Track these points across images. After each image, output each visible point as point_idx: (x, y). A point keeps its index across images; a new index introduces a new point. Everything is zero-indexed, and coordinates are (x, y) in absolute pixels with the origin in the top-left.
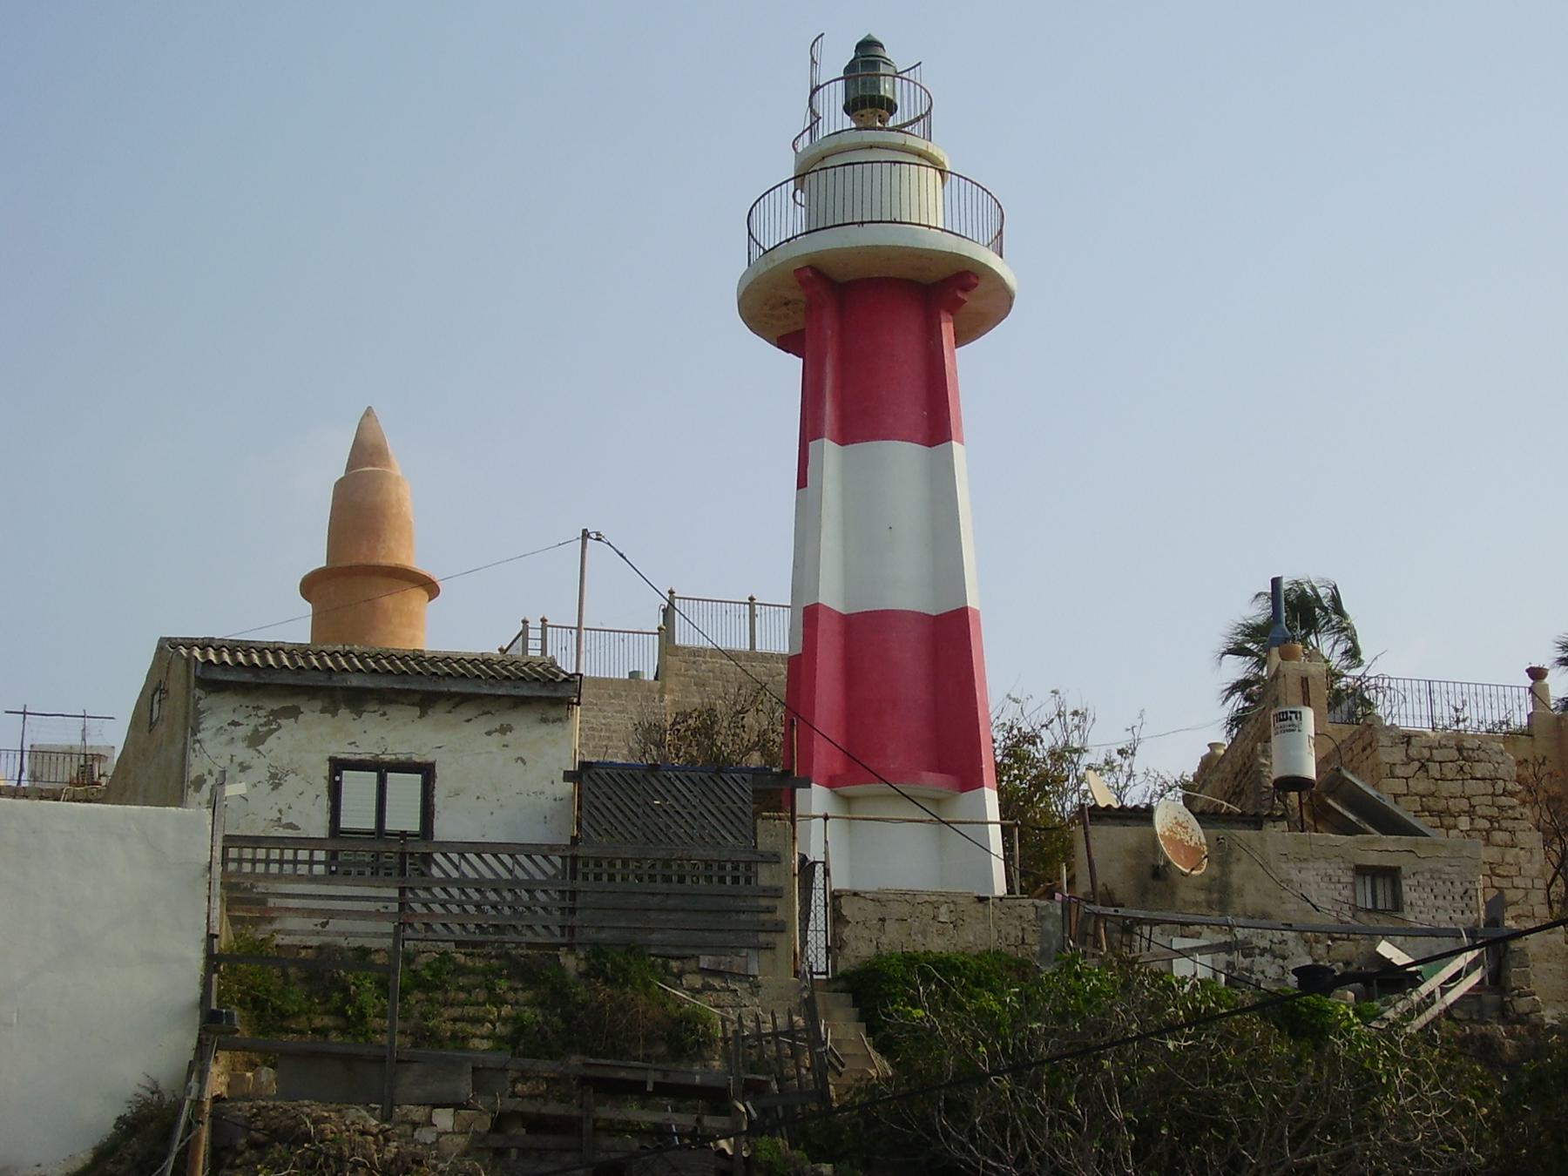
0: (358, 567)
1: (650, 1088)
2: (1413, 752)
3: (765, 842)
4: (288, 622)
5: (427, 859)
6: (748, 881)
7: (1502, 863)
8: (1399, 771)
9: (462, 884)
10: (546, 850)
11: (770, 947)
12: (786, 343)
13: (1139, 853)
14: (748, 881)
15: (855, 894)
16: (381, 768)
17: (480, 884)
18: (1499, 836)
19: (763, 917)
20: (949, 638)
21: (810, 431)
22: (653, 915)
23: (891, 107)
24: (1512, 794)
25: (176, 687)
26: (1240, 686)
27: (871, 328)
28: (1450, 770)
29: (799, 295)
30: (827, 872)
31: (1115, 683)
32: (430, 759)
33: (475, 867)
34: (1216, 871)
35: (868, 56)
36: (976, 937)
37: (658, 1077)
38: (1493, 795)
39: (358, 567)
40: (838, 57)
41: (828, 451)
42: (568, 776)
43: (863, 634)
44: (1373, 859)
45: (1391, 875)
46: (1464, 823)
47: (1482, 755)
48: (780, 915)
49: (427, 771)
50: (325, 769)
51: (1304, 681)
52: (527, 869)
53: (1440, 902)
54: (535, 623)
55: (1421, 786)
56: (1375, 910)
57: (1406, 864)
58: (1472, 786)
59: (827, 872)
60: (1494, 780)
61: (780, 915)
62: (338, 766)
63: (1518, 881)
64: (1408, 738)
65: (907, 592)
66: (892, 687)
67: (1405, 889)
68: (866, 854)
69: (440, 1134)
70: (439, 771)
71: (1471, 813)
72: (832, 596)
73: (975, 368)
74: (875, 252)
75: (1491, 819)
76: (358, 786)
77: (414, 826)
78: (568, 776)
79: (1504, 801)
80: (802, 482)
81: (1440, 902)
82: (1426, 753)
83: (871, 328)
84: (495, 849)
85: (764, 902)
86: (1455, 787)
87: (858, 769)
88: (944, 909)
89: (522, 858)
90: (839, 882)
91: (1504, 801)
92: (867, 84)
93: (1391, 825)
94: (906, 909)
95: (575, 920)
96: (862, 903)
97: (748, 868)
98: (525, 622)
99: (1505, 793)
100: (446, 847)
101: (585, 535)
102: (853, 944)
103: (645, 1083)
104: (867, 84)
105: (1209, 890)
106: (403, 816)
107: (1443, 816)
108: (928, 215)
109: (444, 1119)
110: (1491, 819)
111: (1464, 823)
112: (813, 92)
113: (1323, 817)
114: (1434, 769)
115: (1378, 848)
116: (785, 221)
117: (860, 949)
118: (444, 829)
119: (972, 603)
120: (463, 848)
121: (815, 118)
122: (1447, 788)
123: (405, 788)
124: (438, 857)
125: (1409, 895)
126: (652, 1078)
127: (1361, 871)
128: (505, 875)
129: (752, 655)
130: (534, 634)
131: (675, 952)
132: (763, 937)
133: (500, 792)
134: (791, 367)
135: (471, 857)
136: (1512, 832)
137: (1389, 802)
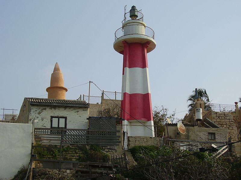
0: (55, 87)
2: (217, 115)
3: (118, 129)
4: (44, 95)
5: (66, 131)
6: (115, 135)
9: (71, 135)
10: (84, 130)
11: (118, 145)
13: (175, 130)
14: (115, 135)
15: (131, 137)
16: (59, 118)
17: (74, 135)
18: (230, 128)
20: (146, 98)
21: (124, 66)
22: (100, 140)
23: (137, 16)
25: (27, 105)
27: (134, 51)
28: (223, 118)
29: (123, 45)
30: (127, 134)
31: (171, 103)
33: (73, 133)
34: (187, 133)
35: (133, 8)
36: (150, 143)
39: (55, 87)
40: (129, 9)
41: (127, 69)
42: (87, 119)
43: (133, 97)
44: (211, 131)
45: (214, 134)
46: (225, 126)
47: (228, 116)
48: (120, 140)
51: (201, 104)
53: (221, 138)
54: (82, 95)
55: (218, 120)
56: (211, 139)
57: (216, 132)
59: (127, 134)
61: (120, 140)
62: (52, 117)
64: (216, 113)
66: (137, 105)
67: (216, 136)
68: (132, 131)
69: (68, 174)
71: (226, 124)
73: (150, 56)
74: (134, 38)
76: (55, 120)
78: (87, 119)
80: (123, 74)
81: (221, 138)
82: (219, 115)
83: (134, 51)
84: (76, 130)
85: (117, 138)
86: (224, 121)
87: (132, 118)
88: (145, 139)
90: (129, 135)
92: (133, 13)
93: (214, 126)
94: (139, 139)
95: (88, 141)
96: (133, 138)
97: (115, 132)
100: (69, 130)
101: (90, 82)
102: (131, 145)
104: (133, 13)
105: (186, 136)
106: (62, 125)
108: (143, 33)
109: (68, 171)
111: (225, 126)
114: (220, 118)
115: (212, 130)
116: (121, 34)
117: (132, 145)
118: (68, 127)
120: (71, 130)
121: (125, 18)
123: (62, 121)
124: (67, 131)
125: (216, 137)
126: (100, 165)
127: (209, 133)
128: (78, 134)
129: (116, 100)
130: (82, 97)
131: (104, 146)
132: (117, 143)
133: (77, 121)
134: (122, 56)
137: (214, 123)
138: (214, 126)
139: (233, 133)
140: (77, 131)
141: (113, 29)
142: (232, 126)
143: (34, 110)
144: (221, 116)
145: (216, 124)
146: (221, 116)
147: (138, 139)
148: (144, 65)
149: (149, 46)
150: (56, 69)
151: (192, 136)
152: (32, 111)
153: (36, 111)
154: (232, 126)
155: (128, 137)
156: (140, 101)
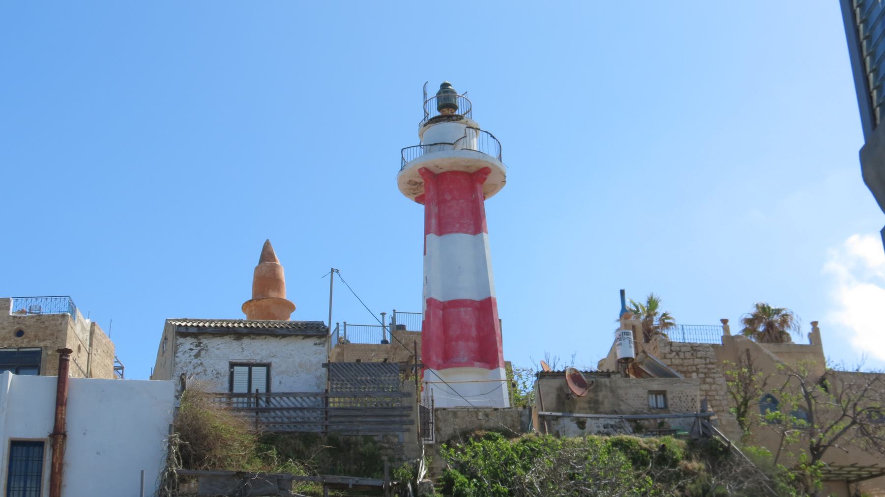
1: (350, 486)
2: (673, 348)
7: (711, 390)
8: (668, 356)
10: (316, 395)
11: (408, 430)
12: (419, 200)
15: (444, 409)
16: (250, 365)
18: (708, 380)
19: (405, 418)
21: (427, 231)
24: (713, 364)
26: (291, 307)
28: (688, 355)
31: (556, 327)
32: (269, 361)
33: (286, 402)
35: (445, 86)
37: (354, 482)
38: (706, 364)
40: (433, 90)
41: (432, 237)
45: (663, 393)
46: (694, 375)
48: (412, 417)
49: (268, 366)
50: (227, 367)
52: (308, 402)
54: (341, 324)
55: (677, 361)
58: (697, 361)
60: (705, 358)
62: (233, 365)
63: (717, 397)
64: (671, 344)
65: (468, 292)
66: (466, 328)
68: (450, 389)
70: (273, 365)
71: (697, 371)
72: (439, 297)
73: (491, 206)
75: (705, 374)
76: (241, 373)
77: (262, 390)
78: (324, 365)
79: (710, 366)
82: (678, 349)
83: (454, 195)
84: (294, 395)
87: (448, 360)
88: (480, 414)
89: (305, 398)
90: (436, 406)
91: (710, 366)
92: (447, 105)
93: (663, 373)
98: (338, 324)
99: (710, 363)
100: (277, 394)
101: (332, 270)
103: (348, 485)
104: (447, 105)
106: (259, 384)
107: (686, 373)
110: (705, 374)
111: (694, 375)
112: (425, 102)
113: (639, 373)
116: (415, 156)
118: (275, 388)
119: (492, 295)
122: (686, 362)
123: (259, 374)
127: (651, 392)
130: (341, 328)
132: (405, 427)
134: (421, 208)
135: (285, 398)
136: (714, 378)
138: (663, 373)
139: (715, 393)
140: (291, 398)
141: (400, 135)
142: (712, 375)
143: (187, 344)
144: (683, 349)
145: (673, 371)
146: (683, 349)
147: (460, 414)
148: (475, 223)
149: (490, 179)
150: (267, 255)
151: (606, 401)
152: (181, 349)
153: (191, 349)
154: (712, 375)
155: (437, 410)
156: (468, 316)
